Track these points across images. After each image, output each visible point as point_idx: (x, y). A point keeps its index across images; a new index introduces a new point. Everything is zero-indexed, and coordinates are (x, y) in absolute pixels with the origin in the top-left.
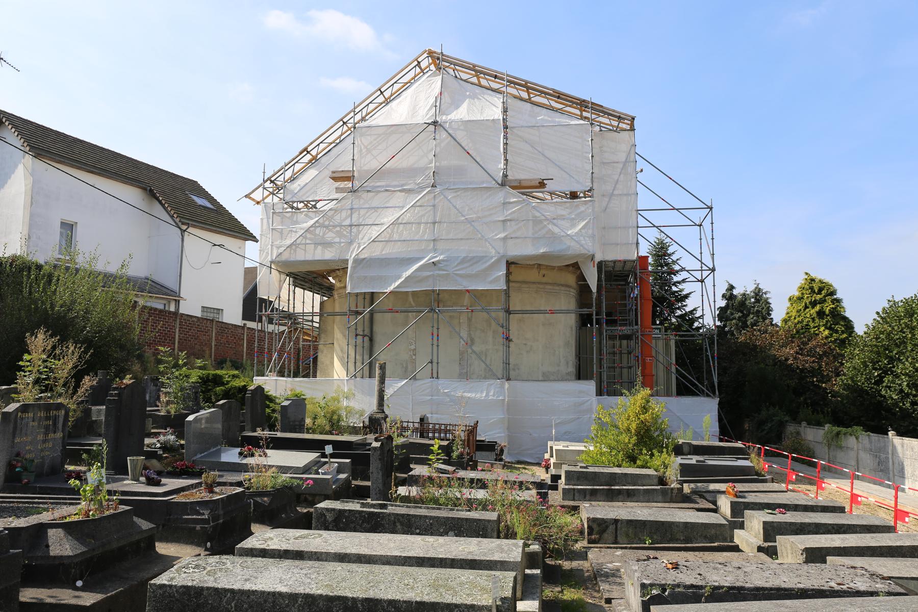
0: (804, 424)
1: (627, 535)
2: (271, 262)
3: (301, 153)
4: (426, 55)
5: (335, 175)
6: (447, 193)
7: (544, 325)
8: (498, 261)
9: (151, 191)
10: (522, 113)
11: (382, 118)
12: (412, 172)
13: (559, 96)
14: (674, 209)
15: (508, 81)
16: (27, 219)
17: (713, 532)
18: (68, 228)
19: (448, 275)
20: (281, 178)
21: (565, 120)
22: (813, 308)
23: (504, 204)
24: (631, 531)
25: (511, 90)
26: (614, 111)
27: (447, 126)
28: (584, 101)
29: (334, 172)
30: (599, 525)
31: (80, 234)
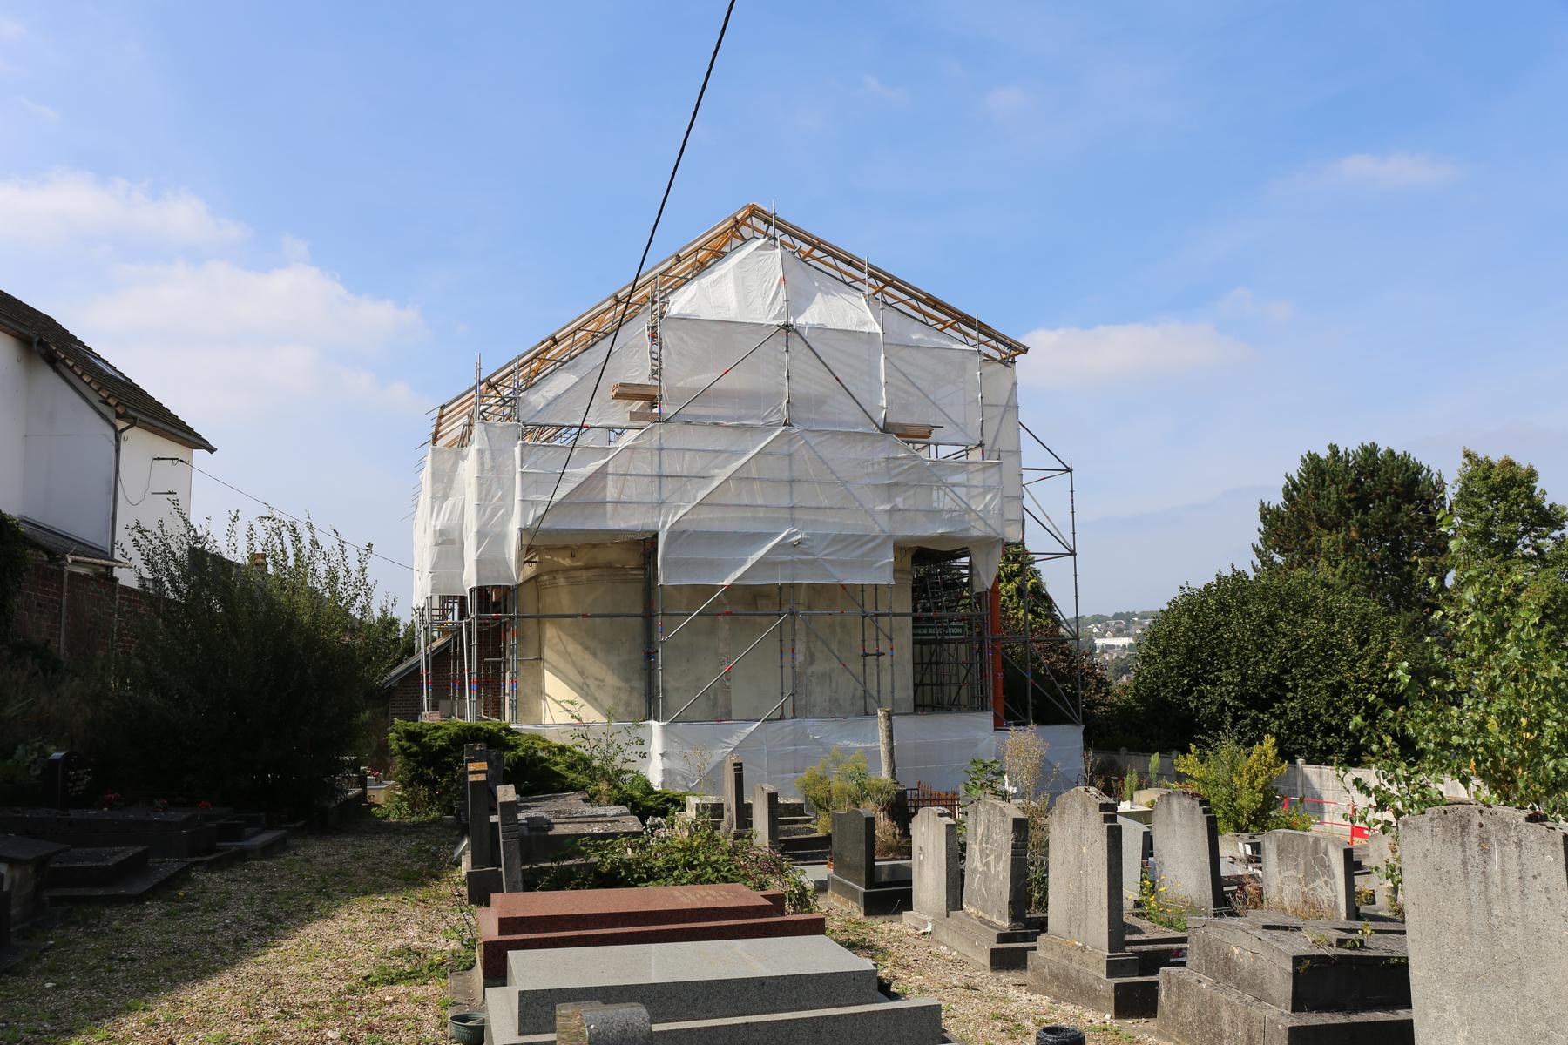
0: (1123, 750)
5: (625, 390)
6: (808, 436)
8: (884, 543)
12: (752, 399)
13: (935, 304)
22: (1009, 581)
27: (805, 333)
29: (623, 385)
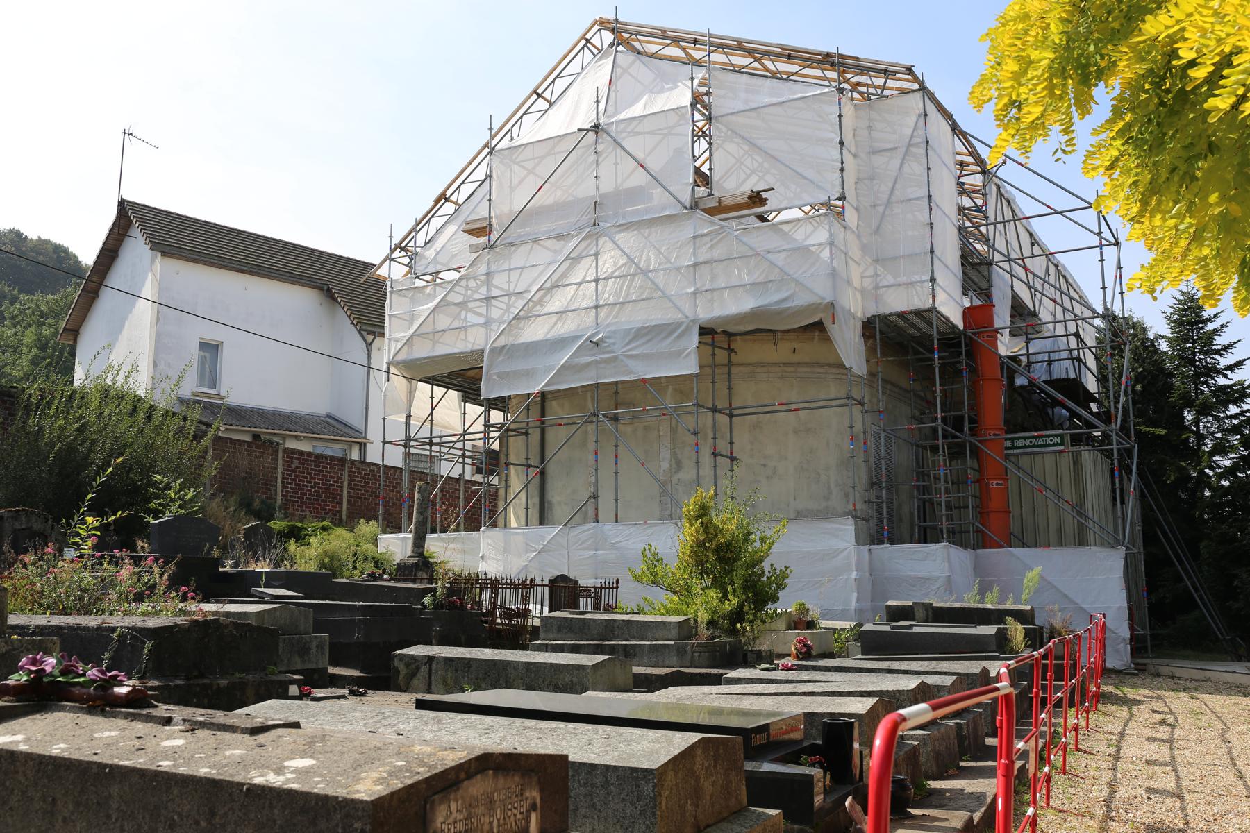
1: (445, 682)
2: (389, 364)
3: (437, 202)
4: (596, 28)
7: (796, 432)
9: (329, 290)
10: (734, 96)
11: (531, 130)
13: (790, 54)
14: (1061, 213)
15: (711, 44)
16: (153, 343)
17: (567, 678)
18: (210, 349)
19: (616, 358)
20: (412, 244)
21: (799, 91)
23: (694, 238)
24: (450, 675)
25: (716, 57)
26: (877, 62)
28: (828, 54)
30: (407, 665)
31: (228, 357)
